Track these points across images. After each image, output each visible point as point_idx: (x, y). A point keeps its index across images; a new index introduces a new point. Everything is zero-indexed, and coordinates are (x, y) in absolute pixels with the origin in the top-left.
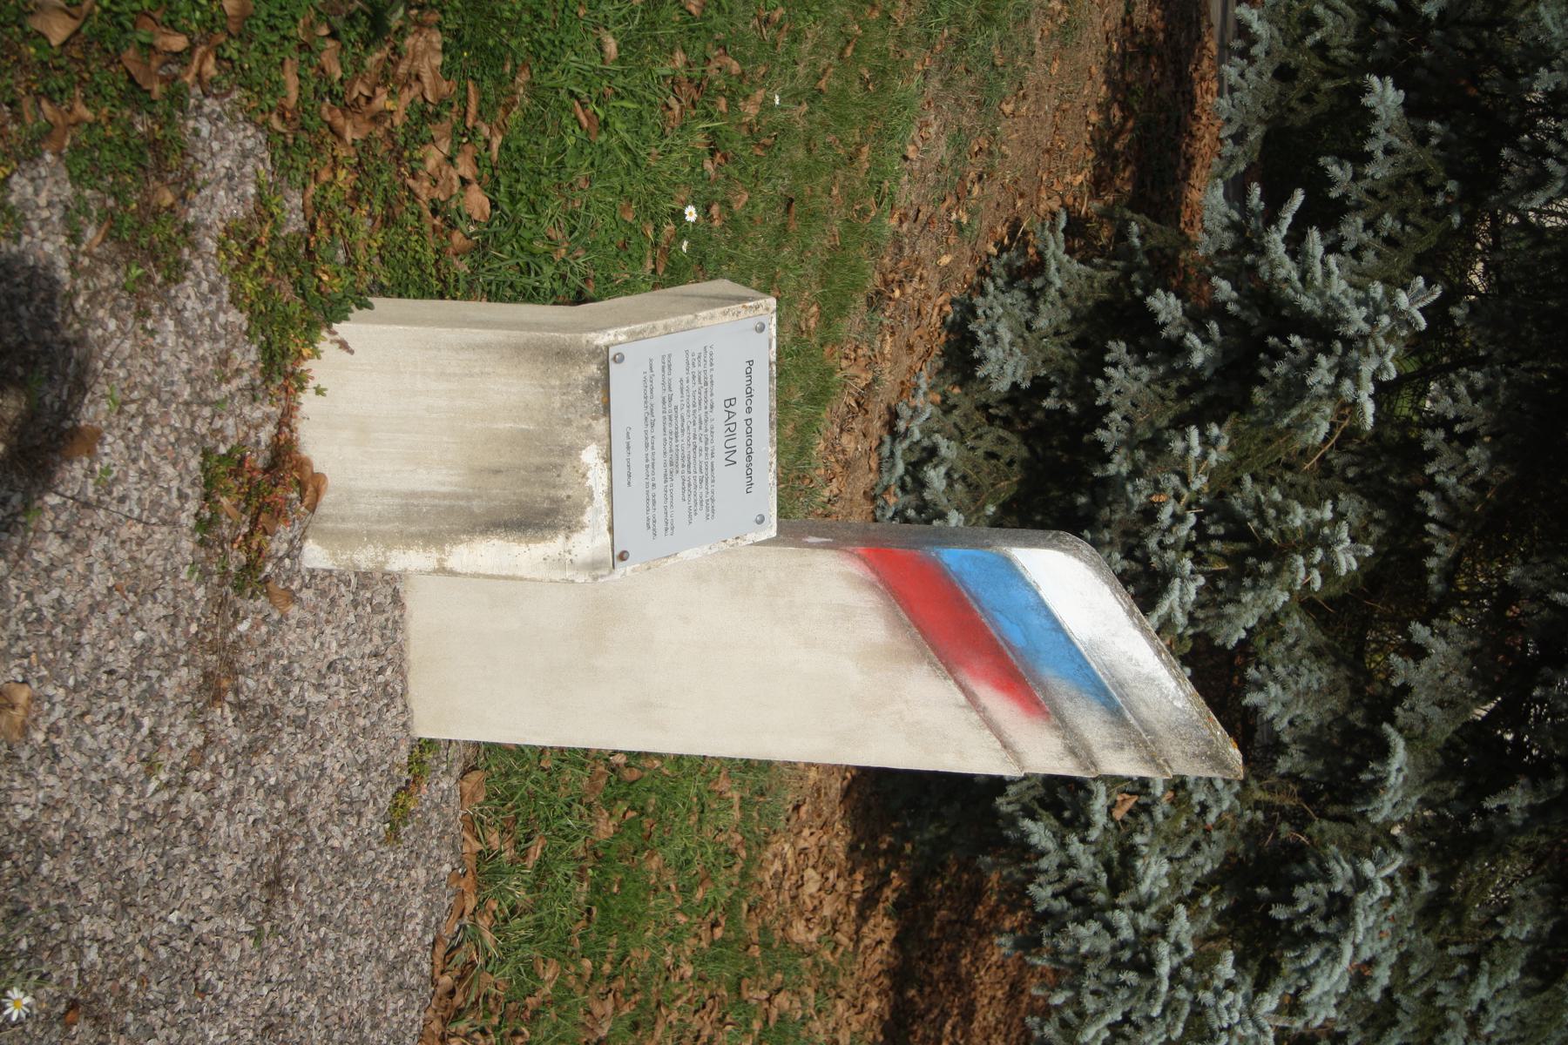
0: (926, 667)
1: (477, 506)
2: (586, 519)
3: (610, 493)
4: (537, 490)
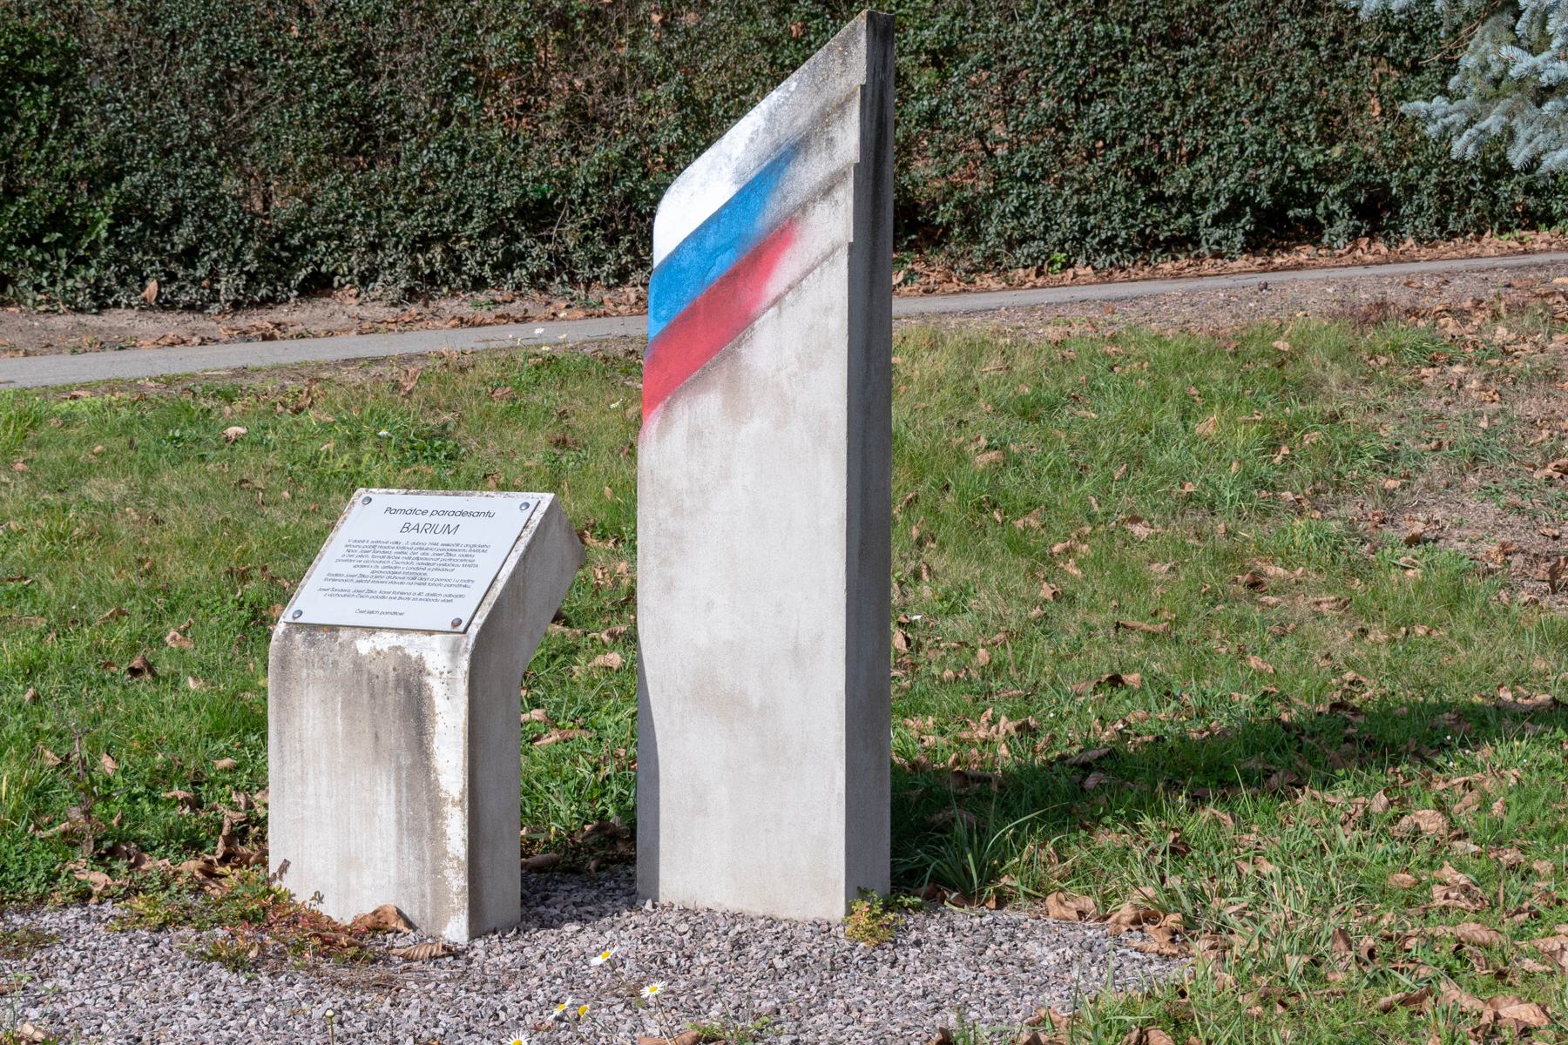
0: (743, 350)
1: (406, 761)
2: (414, 655)
3: (401, 631)
4: (390, 699)
